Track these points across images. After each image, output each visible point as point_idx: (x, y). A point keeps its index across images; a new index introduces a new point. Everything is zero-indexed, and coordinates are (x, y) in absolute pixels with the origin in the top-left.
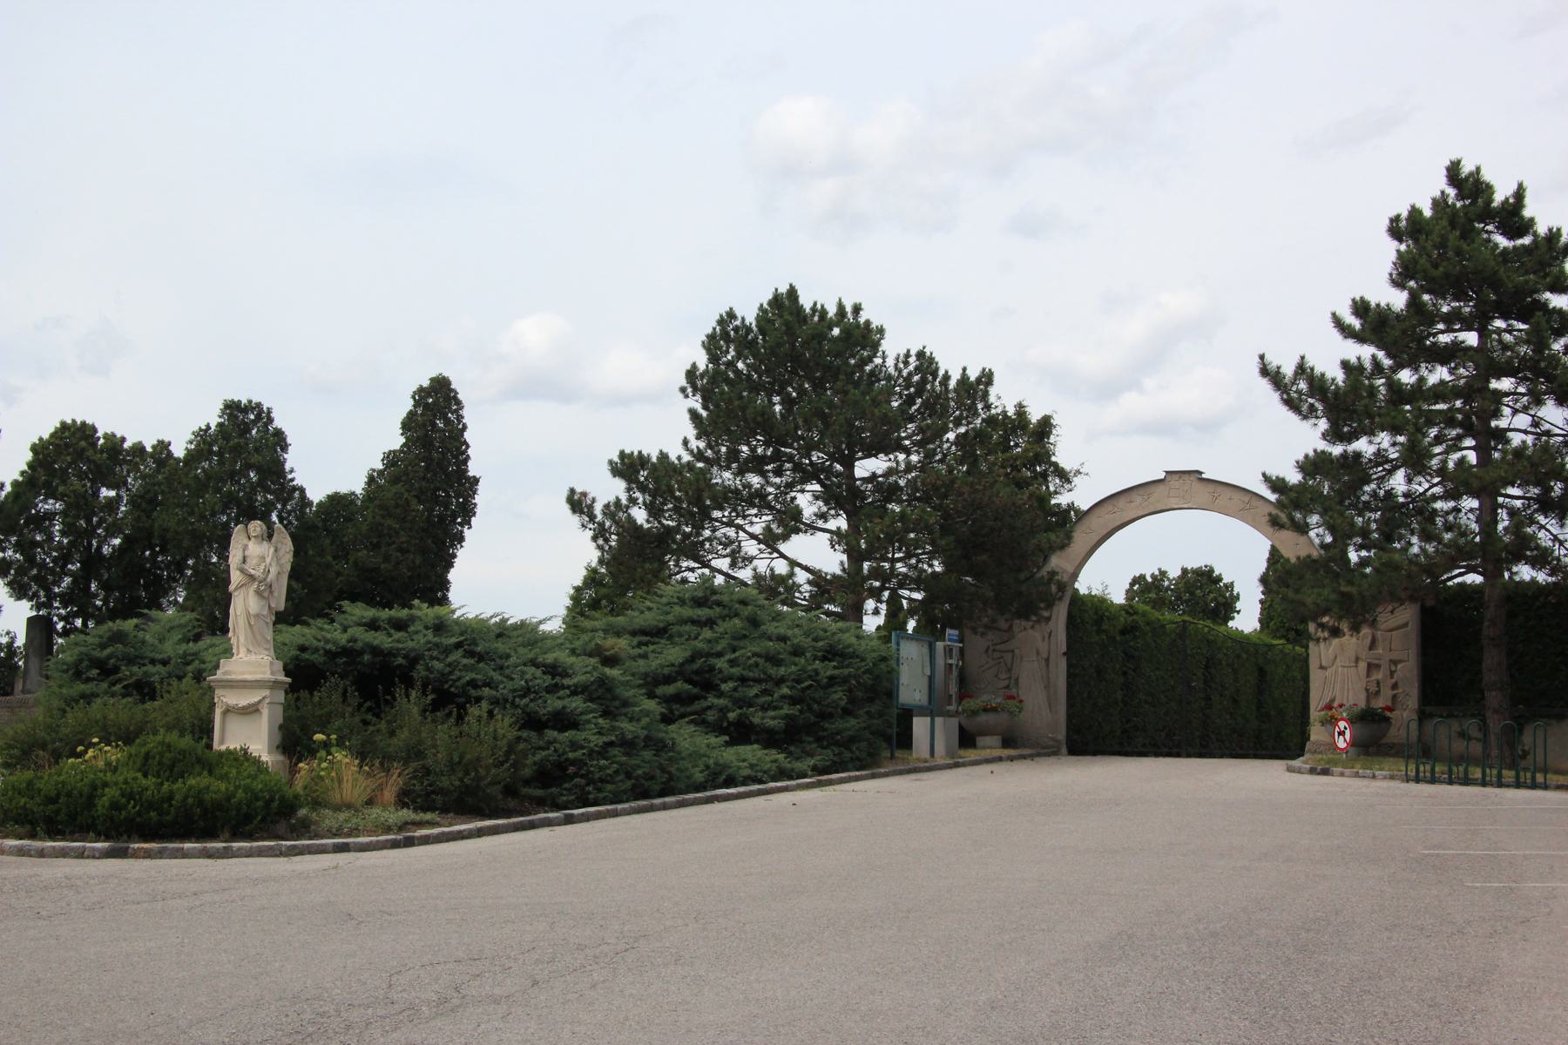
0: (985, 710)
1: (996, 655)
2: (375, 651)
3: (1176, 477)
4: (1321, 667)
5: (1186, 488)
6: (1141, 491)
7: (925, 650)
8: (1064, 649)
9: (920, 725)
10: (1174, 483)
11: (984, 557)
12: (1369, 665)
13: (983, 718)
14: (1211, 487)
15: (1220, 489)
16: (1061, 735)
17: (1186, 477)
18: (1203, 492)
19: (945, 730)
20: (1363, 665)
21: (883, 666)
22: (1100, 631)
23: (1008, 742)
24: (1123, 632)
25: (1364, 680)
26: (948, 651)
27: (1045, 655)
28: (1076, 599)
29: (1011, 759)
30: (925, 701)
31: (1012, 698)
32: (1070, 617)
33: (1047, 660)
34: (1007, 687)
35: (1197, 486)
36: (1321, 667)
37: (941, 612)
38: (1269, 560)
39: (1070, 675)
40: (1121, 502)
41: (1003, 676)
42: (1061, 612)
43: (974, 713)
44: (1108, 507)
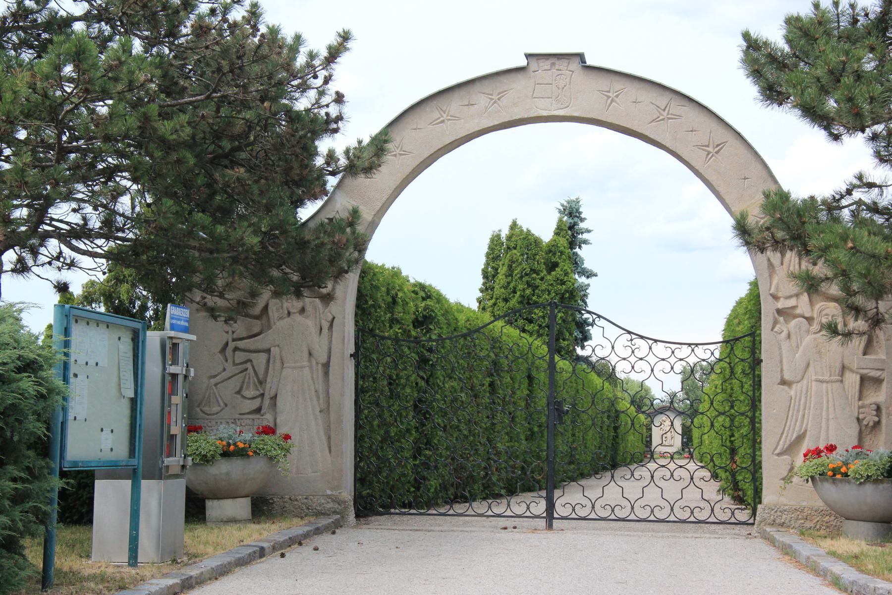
0: (226, 454)
1: (240, 356)
2: (495, 343)
3: (545, 64)
4: (783, 382)
5: (557, 84)
6: (487, 86)
7: (126, 346)
8: (352, 350)
9: (109, 498)
10: (542, 70)
11: (218, 198)
12: (863, 379)
13: (223, 469)
14: (604, 83)
15: (619, 84)
16: (347, 493)
17: (562, 64)
18: (588, 95)
19: (160, 498)
20: (852, 380)
21: (27, 383)
22: (393, 321)
23: (262, 507)
24: (417, 323)
25: (857, 404)
26: (170, 350)
27: (323, 359)
28: (368, 272)
29: (281, 548)
30: (121, 452)
31: (269, 431)
32: (361, 297)
33: (326, 366)
34: (258, 410)
35: (579, 76)
36: (783, 382)
37: (151, 270)
38: (488, 255)
39: (359, 391)
40: (454, 104)
41: (250, 392)
42: (347, 290)
43: (206, 459)
44: (431, 113)
